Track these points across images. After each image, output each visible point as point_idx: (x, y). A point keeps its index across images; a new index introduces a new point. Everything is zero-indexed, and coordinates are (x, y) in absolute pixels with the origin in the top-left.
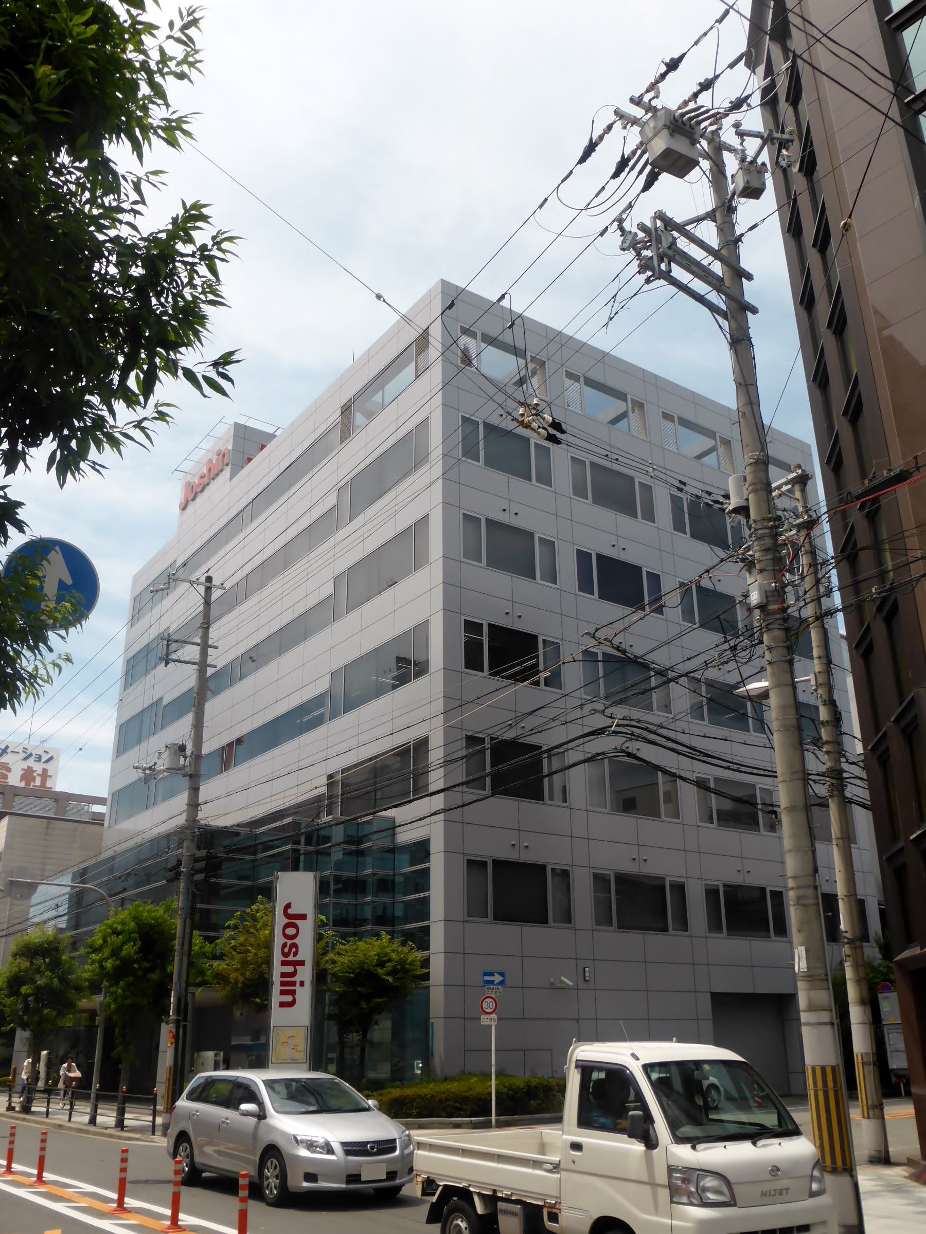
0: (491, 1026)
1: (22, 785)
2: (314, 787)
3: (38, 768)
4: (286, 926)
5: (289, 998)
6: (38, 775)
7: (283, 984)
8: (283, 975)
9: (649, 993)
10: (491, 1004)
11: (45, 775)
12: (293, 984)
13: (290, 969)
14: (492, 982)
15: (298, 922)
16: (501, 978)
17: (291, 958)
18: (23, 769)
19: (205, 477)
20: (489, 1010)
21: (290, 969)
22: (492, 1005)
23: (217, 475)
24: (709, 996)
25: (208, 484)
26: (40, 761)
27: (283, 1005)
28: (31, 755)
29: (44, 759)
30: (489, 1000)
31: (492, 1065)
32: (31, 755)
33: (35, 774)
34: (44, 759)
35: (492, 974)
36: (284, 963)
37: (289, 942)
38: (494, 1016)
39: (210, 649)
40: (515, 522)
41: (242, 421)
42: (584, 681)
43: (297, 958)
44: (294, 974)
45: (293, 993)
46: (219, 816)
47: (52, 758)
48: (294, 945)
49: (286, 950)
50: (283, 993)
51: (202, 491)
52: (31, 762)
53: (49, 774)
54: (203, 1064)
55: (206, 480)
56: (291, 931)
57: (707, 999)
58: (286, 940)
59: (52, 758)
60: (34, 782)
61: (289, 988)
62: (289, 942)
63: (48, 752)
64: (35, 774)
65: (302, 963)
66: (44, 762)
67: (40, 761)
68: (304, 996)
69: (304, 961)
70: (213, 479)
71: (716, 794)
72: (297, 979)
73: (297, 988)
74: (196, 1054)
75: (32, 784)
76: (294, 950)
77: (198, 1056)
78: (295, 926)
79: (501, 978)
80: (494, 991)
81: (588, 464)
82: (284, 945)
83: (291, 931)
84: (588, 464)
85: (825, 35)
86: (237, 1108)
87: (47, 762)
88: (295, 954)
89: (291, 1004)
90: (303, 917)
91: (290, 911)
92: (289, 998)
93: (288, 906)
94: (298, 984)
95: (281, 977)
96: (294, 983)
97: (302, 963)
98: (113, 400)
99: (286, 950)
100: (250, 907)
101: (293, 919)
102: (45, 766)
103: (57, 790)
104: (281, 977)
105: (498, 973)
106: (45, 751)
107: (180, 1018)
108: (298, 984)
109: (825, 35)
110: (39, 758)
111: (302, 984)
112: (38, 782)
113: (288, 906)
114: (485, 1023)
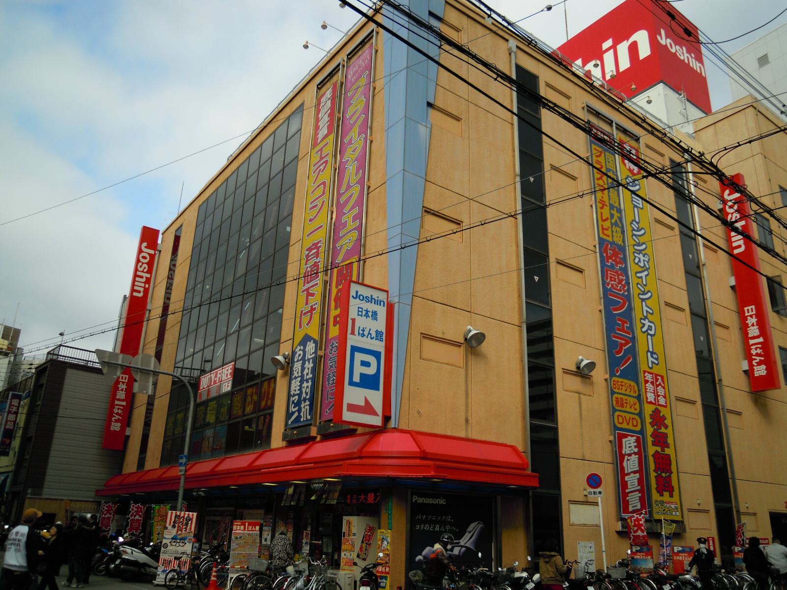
2: (722, 146)
13: (373, 300)
15: (358, 294)
17: (370, 299)
21: (373, 300)
37: (365, 299)
39: (367, 20)
42: (285, 285)
43: (370, 297)
44: (374, 299)
45: (381, 301)
46: (600, 294)
48: (366, 297)
62: (365, 299)
72: (376, 299)
78: (360, 295)
85: (419, 243)
86: (320, 110)
91: (355, 297)
96: (378, 300)
98: (64, 570)
100: (291, 505)
109: (419, 243)
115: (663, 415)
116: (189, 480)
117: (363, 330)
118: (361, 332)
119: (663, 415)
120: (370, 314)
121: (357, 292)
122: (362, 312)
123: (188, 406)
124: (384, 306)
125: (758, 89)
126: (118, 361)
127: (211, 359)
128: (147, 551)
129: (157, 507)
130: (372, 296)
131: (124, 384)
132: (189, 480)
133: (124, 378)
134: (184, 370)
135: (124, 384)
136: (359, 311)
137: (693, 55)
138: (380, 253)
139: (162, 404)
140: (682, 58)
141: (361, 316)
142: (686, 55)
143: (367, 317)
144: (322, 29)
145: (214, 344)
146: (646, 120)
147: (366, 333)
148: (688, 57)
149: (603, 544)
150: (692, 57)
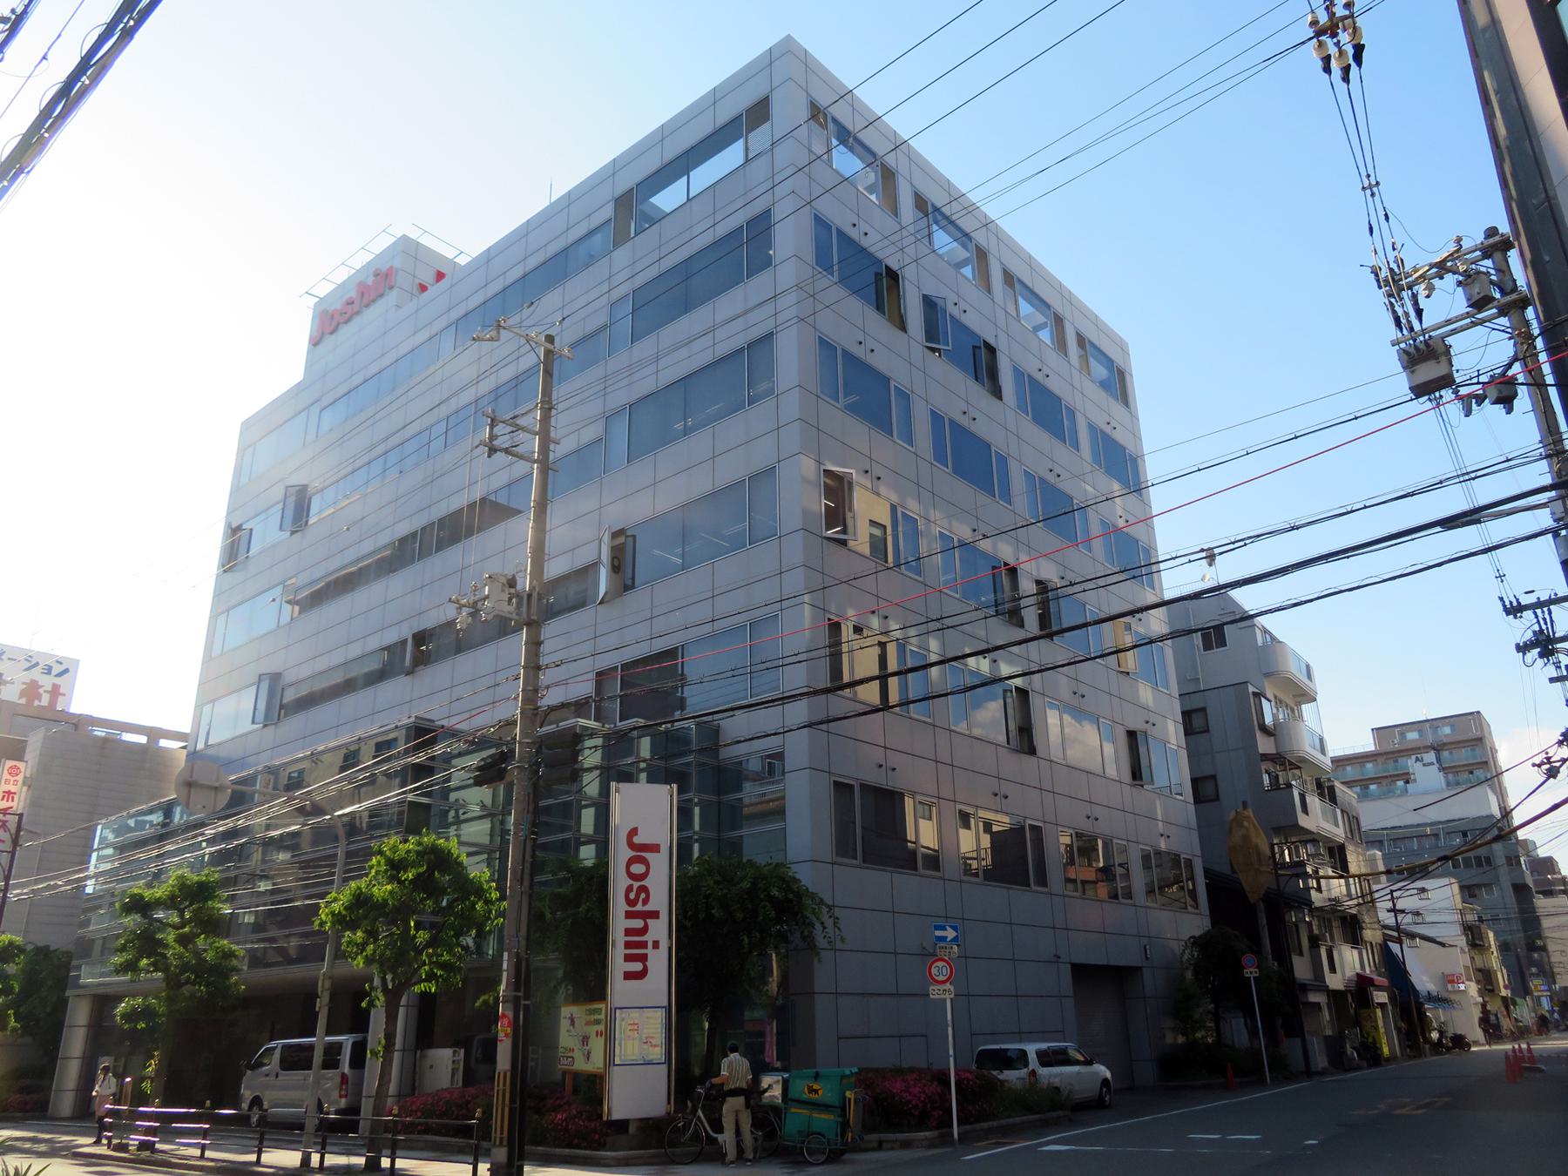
0: (945, 1000)
1: (23, 701)
3: (47, 682)
4: (630, 862)
5: (638, 967)
6: (45, 691)
7: (628, 945)
8: (628, 932)
9: (968, 960)
10: (944, 968)
11: (55, 692)
12: (644, 945)
13: (638, 923)
14: (943, 939)
16: (954, 934)
17: (639, 907)
18: (24, 683)
19: (353, 303)
20: (941, 978)
21: (638, 923)
22: (946, 971)
23: (374, 301)
24: (1069, 966)
25: (358, 313)
26: (49, 673)
27: (629, 976)
28: (37, 664)
29: (54, 672)
30: (940, 964)
31: (949, 1056)
32: (37, 664)
33: (41, 691)
34: (54, 672)
35: (943, 928)
36: (629, 915)
37: (636, 885)
38: (947, 986)
40: (872, 360)
41: (413, 234)
43: (648, 908)
44: (644, 930)
45: (643, 958)
47: (66, 671)
48: (644, 889)
49: (632, 896)
50: (628, 958)
51: (347, 322)
52: (36, 674)
53: (61, 691)
54: (431, 1067)
55: (356, 307)
56: (638, 869)
57: (1066, 971)
58: (631, 882)
59: (66, 671)
60: (40, 701)
61: (637, 949)
62: (636, 885)
63: (61, 663)
64: (41, 691)
65: (655, 915)
66: (56, 676)
67: (49, 673)
68: (659, 963)
69: (659, 912)
70: (367, 306)
71: (492, 828)
72: (649, 938)
73: (649, 951)
74: (418, 1052)
75: (36, 703)
76: (643, 896)
77: (423, 1057)
79: (954, 934)
80: (947, 951)
81: (839, 352)
82: (629, 889)
83: (638, 869)
84: (839, 352)
87: (59, 675)
88: (645, 902)
89: (641, 975)
90: (655, 848)
91: (636, 840)
92: (638, 967)
93: (634, 832)
94: (650, 945)
95: (626, 935)
96: (644, 945)
97: (655, 915)
99: (632, 896)
101: (641, 851)
102: (58, 681)
103: (71, 711)
104: (626, 935)
105: (951, 927)
106: (58, 662)
107: (521, 994)
108: (650, 945)
110: (48, 670)
111: (656, 945)
112: (45, 701)
113: (634, 832)
114: (937, 996)
115: (1561, 736)
119: (1561, 736)
123: (1498, 96)
125: (270, 510)
126: (1374, 884)
127: (840, 1041)
129: (1169, 1039)
134: (893, 682)
138: (796, 653)
139: (1172, 731)
145: (871, 459)
149: (1054, 1137)
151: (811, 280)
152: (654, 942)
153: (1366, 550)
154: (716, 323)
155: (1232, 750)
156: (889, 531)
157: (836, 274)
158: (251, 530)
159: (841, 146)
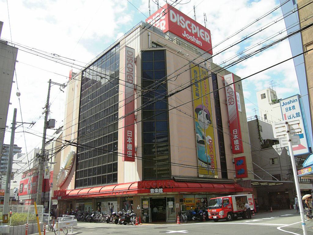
4: (286, 103)
5: (296, 100)
13: (291, 102)
21: (291, 102)
44: (292, 101)
45: (295, 100)
48: (288, 103)
56: (286, 104)
81: (118, 103)
83: (286, 104)
92: (296, 100)
116: (166, 172)
117: (290, 116)
118: (289, 118)
120: (291, 108)
121: (283, 103)
122: (288, 109)
124: (297, 101)
128: (189, 20)
130: (290, 100)
131: (128, 139)
132: (166, 172)
133: (129, 133)
135: (128, 139)
136: (286, 110)
137: (197, 39)
140: (192, 40)
141: (288, 111)
142: (194, 39)
143: (290, 110)
144: (15, 108)
146: (156, 45)
147: (291, 117)
148: (195, 40)
150: (197, 39)
151: (51, 150)
152: (265, 98)
153: (208, 180)
154: (53, 147)
155: (268, 164)
156: (131, 72)
157: (23, 180)
158: (153, 42)
159: (120, 78)
